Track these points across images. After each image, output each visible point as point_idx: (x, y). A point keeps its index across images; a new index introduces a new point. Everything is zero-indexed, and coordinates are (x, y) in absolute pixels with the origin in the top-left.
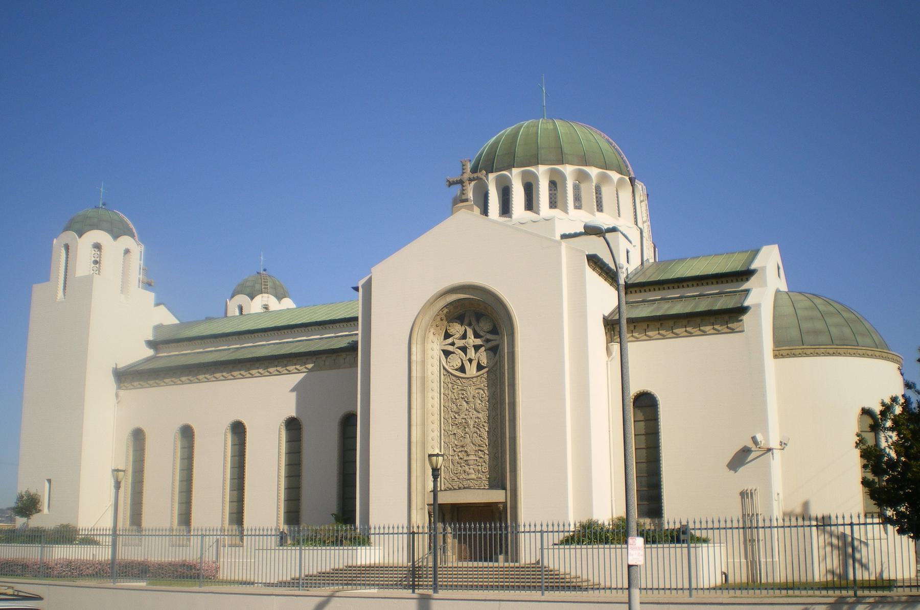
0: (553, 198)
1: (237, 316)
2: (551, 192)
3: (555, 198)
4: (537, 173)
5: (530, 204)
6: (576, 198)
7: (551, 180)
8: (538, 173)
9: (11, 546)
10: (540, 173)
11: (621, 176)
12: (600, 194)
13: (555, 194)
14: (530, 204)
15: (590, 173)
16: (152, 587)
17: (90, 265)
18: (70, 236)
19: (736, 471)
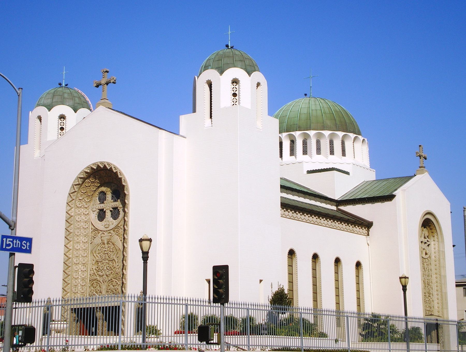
0: (305, 149)
1: (119, 337)
2: (331, 146)
3: (306, 149)
4: (282, 138)
5: (292, 152)
6: (344, 151)
7: (291, 140)
8: (282, 136)
9: (30, 307)
10: (297, 136)
11: (356, 135)
12: (330, 147)
13: (306, 147)
14: (292, 152)
15: (310, 135)
16: (43, 310)
17: (231, 98)
18: (211, 74)
19: (233, 78)
